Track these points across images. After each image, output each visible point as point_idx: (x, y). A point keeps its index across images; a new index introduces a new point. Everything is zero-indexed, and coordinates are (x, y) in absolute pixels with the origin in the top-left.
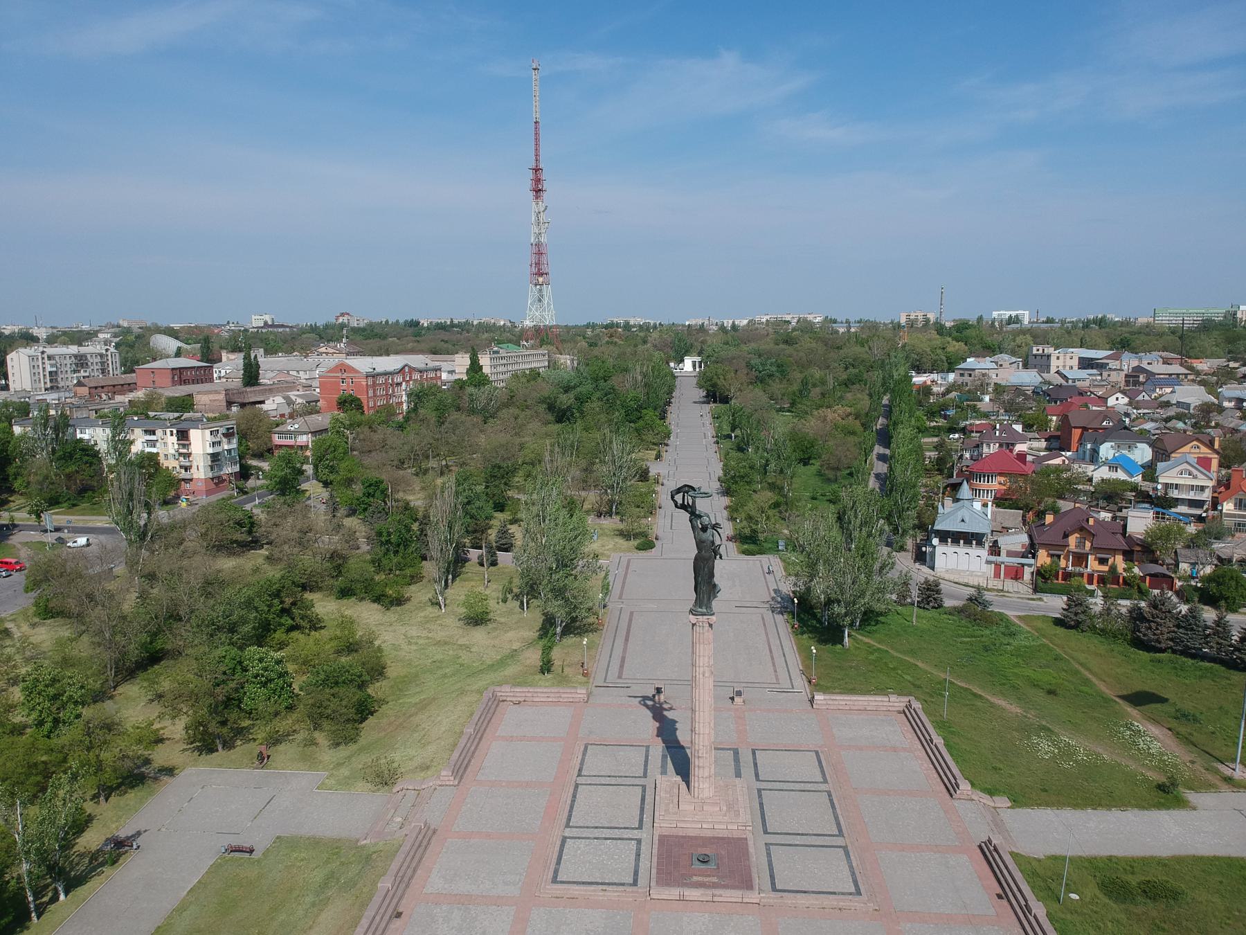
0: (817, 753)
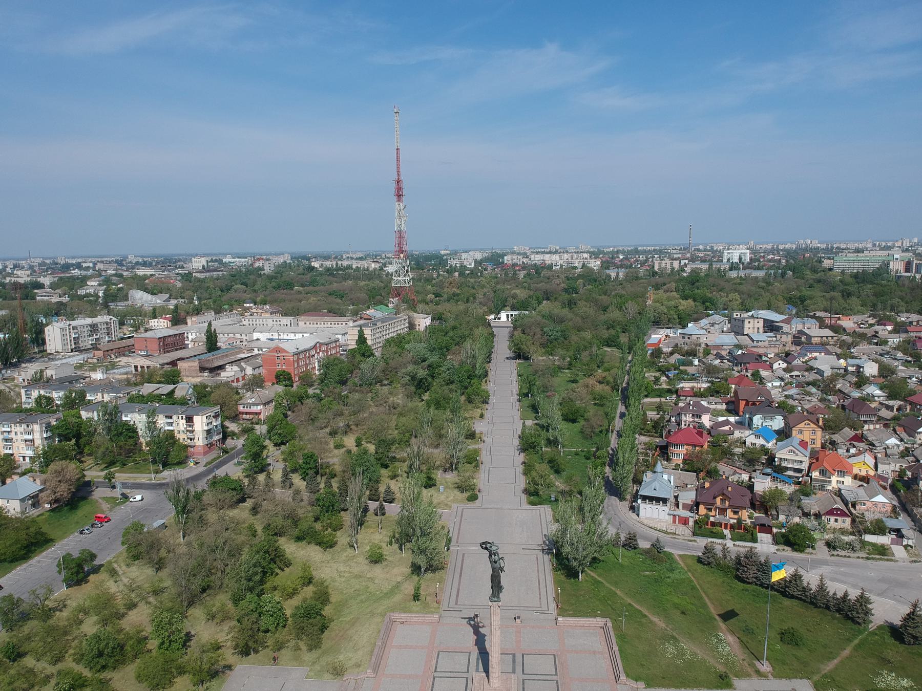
0: (554, 656)
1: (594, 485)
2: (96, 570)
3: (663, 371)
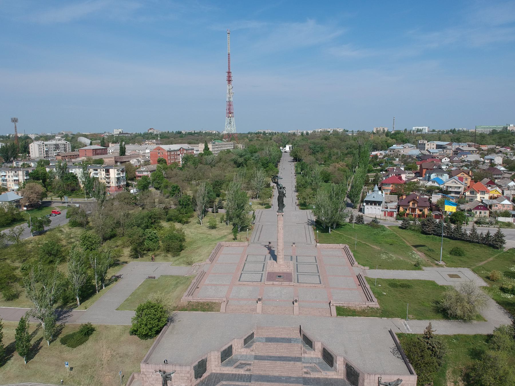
0: (315, 257)
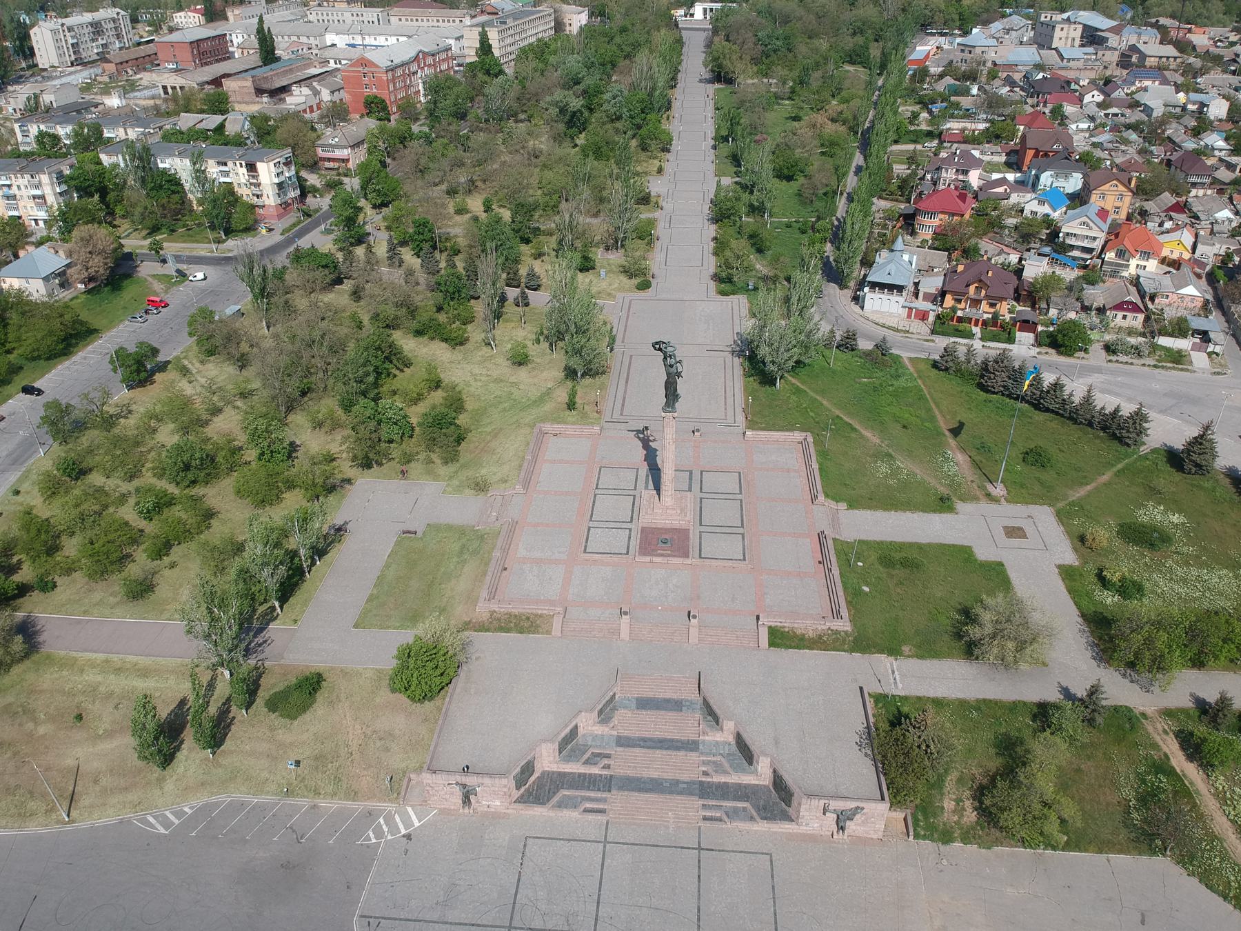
1: (808, 268)
2: (163, 367)
3: (925, 103)
